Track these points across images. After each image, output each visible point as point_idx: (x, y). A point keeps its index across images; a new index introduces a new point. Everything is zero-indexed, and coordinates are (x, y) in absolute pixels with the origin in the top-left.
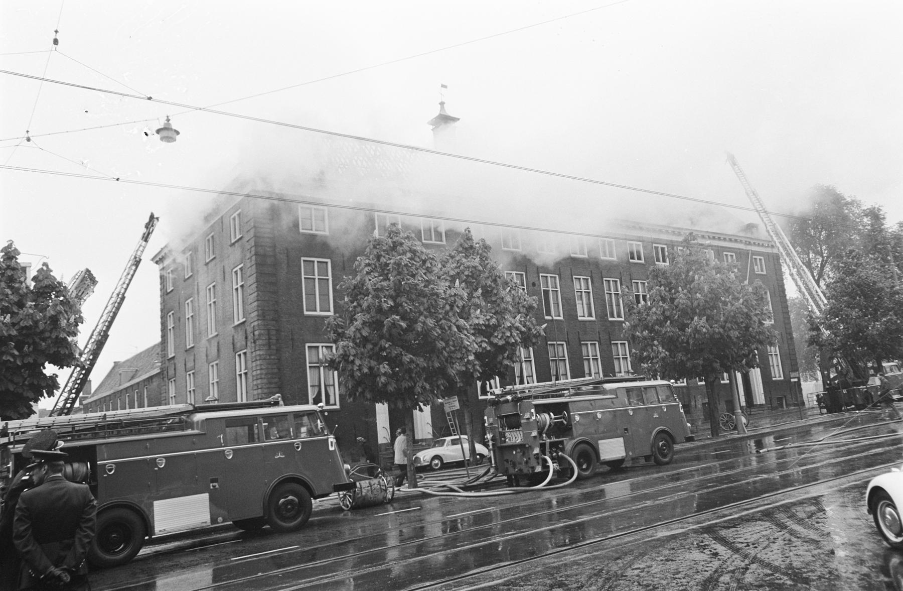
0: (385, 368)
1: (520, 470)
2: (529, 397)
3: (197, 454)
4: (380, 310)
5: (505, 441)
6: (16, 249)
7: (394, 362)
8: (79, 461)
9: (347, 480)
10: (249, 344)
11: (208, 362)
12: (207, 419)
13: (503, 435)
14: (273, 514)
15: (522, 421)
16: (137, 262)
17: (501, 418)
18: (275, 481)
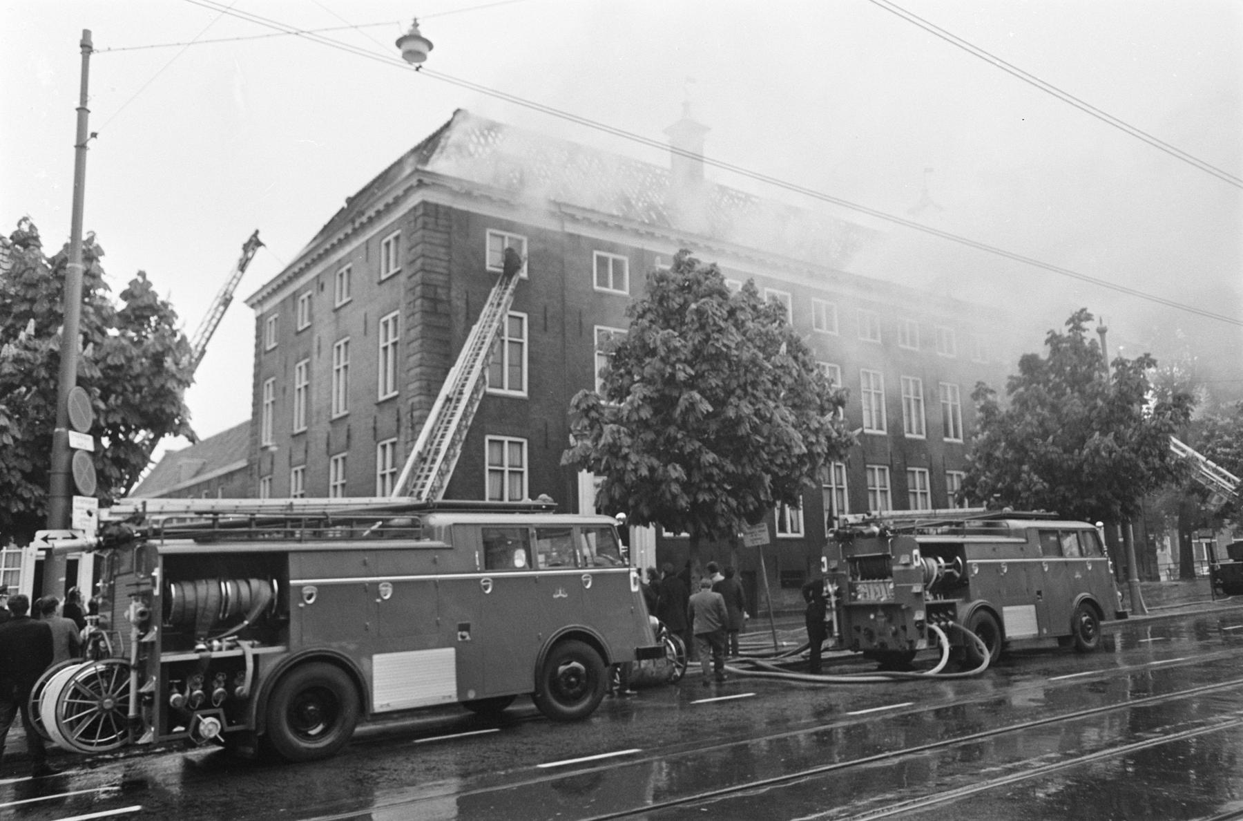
0: (676, 471)
1: (883, 644)
2: (909, 531)
3: (442, 581)
4: (671, 380)
5: (855, 598)
6: (98, 247)
7: (690, 463)
8: (259, 577)
9: (652, 644)
10: (402, 429)
11: (329, 454)
12: (455, 524)
13: (853, 588)
14: (546, 686)
15: (895, 568)
16: (226, 302)
17: (852, 561)
18: (553, 635)
